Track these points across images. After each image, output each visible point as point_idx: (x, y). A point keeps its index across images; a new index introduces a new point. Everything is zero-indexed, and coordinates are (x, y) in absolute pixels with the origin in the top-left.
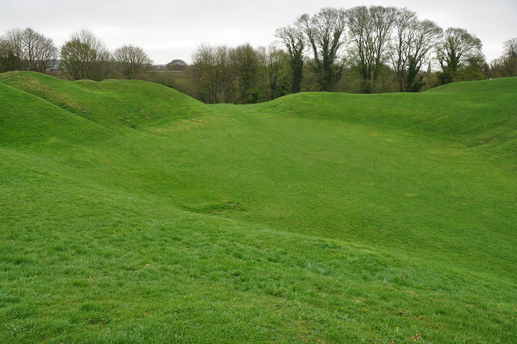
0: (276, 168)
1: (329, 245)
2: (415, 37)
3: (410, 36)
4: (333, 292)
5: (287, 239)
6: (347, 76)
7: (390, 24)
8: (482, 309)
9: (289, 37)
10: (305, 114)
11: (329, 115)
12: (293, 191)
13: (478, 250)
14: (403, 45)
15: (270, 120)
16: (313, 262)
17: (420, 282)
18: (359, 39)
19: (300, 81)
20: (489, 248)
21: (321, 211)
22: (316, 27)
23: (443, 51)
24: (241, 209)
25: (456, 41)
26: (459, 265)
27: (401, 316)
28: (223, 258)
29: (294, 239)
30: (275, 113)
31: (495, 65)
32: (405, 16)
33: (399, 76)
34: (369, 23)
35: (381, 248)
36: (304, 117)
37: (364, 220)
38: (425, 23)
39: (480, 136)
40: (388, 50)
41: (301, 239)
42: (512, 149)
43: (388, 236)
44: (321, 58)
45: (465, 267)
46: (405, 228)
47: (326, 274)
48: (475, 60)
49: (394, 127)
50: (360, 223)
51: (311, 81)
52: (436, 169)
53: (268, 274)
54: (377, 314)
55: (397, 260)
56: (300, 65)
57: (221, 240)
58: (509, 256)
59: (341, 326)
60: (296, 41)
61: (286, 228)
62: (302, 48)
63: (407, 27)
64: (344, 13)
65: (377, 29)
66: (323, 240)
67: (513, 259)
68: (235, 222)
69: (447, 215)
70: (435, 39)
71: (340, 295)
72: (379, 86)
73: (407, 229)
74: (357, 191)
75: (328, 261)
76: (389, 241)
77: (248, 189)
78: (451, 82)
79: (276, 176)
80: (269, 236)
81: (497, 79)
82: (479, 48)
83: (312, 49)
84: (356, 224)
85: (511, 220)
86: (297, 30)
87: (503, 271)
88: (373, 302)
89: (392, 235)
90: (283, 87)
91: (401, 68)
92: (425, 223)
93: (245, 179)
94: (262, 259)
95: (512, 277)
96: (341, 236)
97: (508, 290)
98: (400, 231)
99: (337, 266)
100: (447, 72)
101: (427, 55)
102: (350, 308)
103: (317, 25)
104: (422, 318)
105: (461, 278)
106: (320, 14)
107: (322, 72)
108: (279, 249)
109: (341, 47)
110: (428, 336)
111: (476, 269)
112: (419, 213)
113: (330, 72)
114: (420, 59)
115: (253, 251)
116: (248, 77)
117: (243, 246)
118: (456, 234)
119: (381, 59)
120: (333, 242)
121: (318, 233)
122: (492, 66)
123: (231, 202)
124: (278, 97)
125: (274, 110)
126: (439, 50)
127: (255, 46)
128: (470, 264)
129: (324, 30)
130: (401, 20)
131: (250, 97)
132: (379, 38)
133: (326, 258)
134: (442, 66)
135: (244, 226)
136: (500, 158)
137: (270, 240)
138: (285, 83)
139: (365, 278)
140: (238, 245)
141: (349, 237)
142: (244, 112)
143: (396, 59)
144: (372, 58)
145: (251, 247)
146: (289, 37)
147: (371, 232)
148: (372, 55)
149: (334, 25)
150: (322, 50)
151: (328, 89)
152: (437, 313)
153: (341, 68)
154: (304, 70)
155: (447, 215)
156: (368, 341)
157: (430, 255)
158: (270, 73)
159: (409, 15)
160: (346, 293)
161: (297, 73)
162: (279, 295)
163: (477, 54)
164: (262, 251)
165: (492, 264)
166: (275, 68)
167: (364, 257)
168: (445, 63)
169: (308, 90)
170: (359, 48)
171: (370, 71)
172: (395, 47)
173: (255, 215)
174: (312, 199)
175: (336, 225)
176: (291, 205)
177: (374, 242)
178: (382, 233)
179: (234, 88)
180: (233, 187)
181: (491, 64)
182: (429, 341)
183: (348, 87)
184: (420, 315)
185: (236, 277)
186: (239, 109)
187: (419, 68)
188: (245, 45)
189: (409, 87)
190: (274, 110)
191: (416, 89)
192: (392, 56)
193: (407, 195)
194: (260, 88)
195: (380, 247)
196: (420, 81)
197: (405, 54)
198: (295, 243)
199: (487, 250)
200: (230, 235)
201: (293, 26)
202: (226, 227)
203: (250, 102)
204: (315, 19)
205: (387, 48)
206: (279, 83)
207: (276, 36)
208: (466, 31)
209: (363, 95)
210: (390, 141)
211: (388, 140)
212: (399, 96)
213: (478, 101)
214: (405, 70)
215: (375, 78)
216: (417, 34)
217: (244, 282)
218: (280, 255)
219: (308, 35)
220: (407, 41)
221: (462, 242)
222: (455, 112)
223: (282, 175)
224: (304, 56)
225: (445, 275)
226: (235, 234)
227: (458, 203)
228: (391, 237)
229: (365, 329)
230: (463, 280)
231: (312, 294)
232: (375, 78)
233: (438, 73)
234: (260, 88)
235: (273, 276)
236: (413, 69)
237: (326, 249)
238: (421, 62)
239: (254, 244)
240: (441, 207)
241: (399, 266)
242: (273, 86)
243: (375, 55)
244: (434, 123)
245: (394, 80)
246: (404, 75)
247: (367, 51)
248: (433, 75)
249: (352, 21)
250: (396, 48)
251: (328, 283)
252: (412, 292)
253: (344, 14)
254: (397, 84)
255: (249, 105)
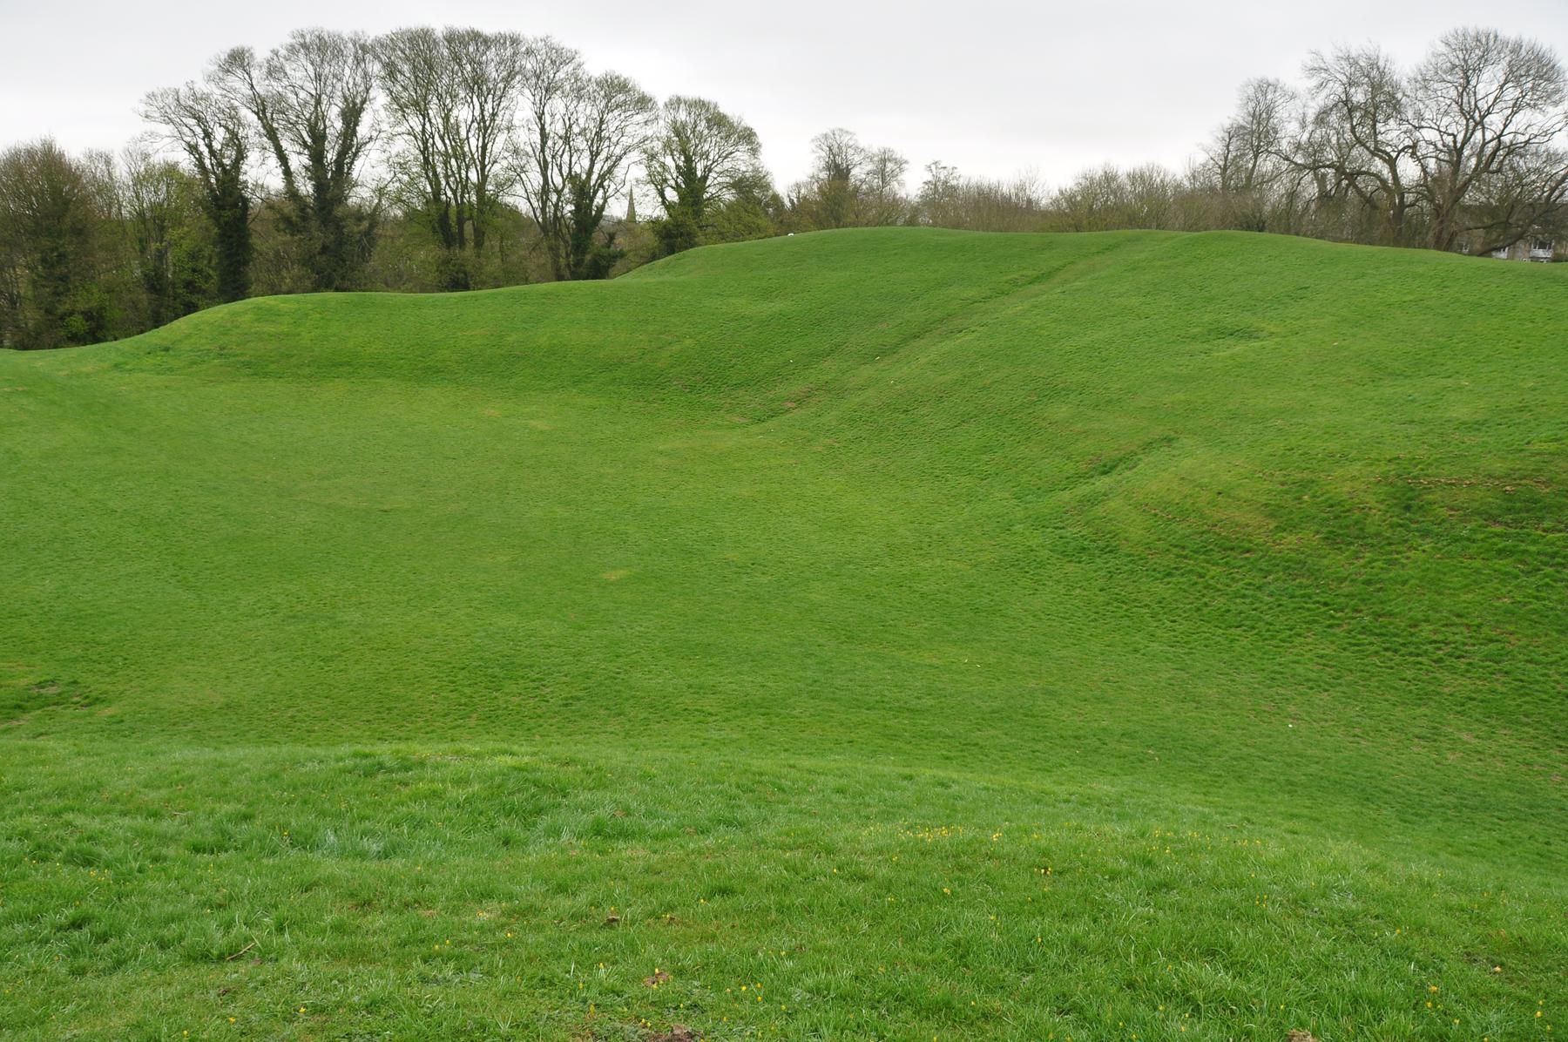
0: (194, 547)
1: (388, 765)
2: (581, 121)
3: (569, 119)
4: (407, 905)
5: (248, 770)
6: (392, 242)
7: (508, 80)
8: (823, 855)
9: (192, 122)
10: (273, 367)
11: (349, 364)
12: (260, 612)
13: (813, 698)
14: (550, 143)
15: (155, 394)
16: (341, 828)
17: (665, 819)
18: (421, 127)
19: (245, 263)
20: (836, 688)
21: (357, 662)
22: (280, 89)
23: (662, 159)
24: (87, 701)
25: (693, 132)
26: (769, 748)
27: (612, 928)
28: (24, 877)
29: (271, 766)
30: (171, 370)
31: (798, 198)
32: (548, 61)
33: (546, 234)
34: (446, 80)
35: (551, 743)
36: (266, 375)
37: (490, 670)
38: (607, 81)
39: (782, 390)
40: (511, 161)
41: (296, 762)
42: (861, 417)
43: (566, 705)
44: (306, 187)
45: (786, 750)
46: (612, 674)
47: (385, 855)
48: (747, 186)
49: (549, 385)
50: (479, 680)
51: (279, 262)
52: (675, 492)
53: (192, 895)
54: (542, 940)
55: (596, 769)
56: (238, 212)
57: (12, 817)
58: (886, 699)
59: (435, 1003)
60: (220, 135)
61: (251, 735)
62: (241, 156)
63: (558, 92)
64: (363, 47)
65: (471, 98)
66: (367, 751)
67: (897, 704)
68: (65, 748)
69: (723, 617)
70: (634, 128)
71: (429, 908)
72: (493, 265)
73: (618, 673)
74: (461, 586)
75: (388, 812)
76: (573, 719)
77: (105, 630)
78: (692, 246)
79: (196, 575)
80: (188, 772)
81: (806, 234)
82: (754, 151)
83: (273, 160)
84: (470, 685)
85: (881, 603)
86: (220, 98)
87: (878, 741)
88: (531, 907)
89: (579, 699)
90: (189, 285)
91: (550, 210)
92: (665, 648)
93: (89, 599)
94: (170, 852)
95: (898, 752)
96: (428, 729)
97: (890, 788)
98: (601, 684)
99: (418, 824)
100: (680, 218)
101: (619, 172)
102: (461, 943)
103: (285, 82)
104: (671, 919)
105: (774, 784)
106: (292, 50)
107: (313, 230)
108: (228, 808)
109: (366, 153)
110: (689, 965)
111: (813, 750)
112: (645, 625)
113: (339, 228)
114: (602, 183)
115: (137, 832)
116: (62, 256)
117: (97, 820)
118: (750, 664)
119: (490, 187)
120: (398, 752)
121: (357, 733)
122: (791, 201)
123: (47, 681)
124: (177, 317)
125: (165, 359)
126: (652, 157)
127: (74, 149)
128: (797, 740)
129: (308, 98)
130: (538, 72)
131: (78, 323)
132: (479, 124)
133: (381, 805)
134: (663, 203)
135: (98, 755)
136: (837, 445)
137: (194, 783)
138: (194, 270)
139: (506, 843)
140: (80, 820)
141: (454, 728)
142: (60, 373)
143: (535, 184)
144: (464, 185)
145: (127, 821)
146: (194, 121)
147: (517, 700)
148: (463, 176)
149: (339, 86)
150: (307, 161)
151: (337, 283)
152: (710, 896)
153: (371, 219)
154: (254, 226)
155: (723, 617)
156: (518, 1026)
157: (691, 736)
158: (141, 241)
159: (559, 58)
160: (447, 898)
161: (231, 237)
162: (232, 955)
163: (751, 168)
164: (167, 826)
165: (850, 728)
166: (154, 222)
167: (498, 780)
168: (672, 195)
169: (274, 290)
170: (423, 153)
171: (460, 222)
172: (529, 149)
173: (139, 712)
174: (324, 629)
175: (409, 699)
176: (258, 658)
177: (529, 730)
178: (549, 697)
179: (11, 295)
180: (48, 632)
181: (789, 196)
182: (694, 978)
183: (400, 275)
184: (666, 912)
185: (76, 934)
186: (39, 364)
187: (601, 209)
188: (38, 145)
189: (578, 264)
190: (165, 359)
191: (599, 270)
192: (523, 175)
193: (605, 576)
194: (108, 292)
195: (549, 739)
196: (609, 247)
197: (560, 170)
198: (276, 777)
199: (833, 693)
200: (46, 796)
201: (202, 87)
202: (32, 769)
203: (76, 339)
204: (275, 63)
205: (506, 154)
206: (174, 272)
207: (147, 117)
208: (716, 107)
209: (449, 294)
210: (540, 424)
211: (533, 423)
212: (551, 294)
213: (766, 295)
214: (563, 216)
215: (479, 244)
216: (588, 112)
217: (105, 941)
218: (230, 827)
219: (257, 114)
220: (562, 132)
221: (769, 684)
222: (710, 329)
223: (216, 568)
224: (250, 181)
225: (730, 786)
226: (65, 789)
227: (745, 579)
228: (578, 705)
229: (509, 995)
230: (779, 789)
231: (339, 928)
232: (479, 244)
233: (655, 222)
234: (109, 291)
235: (209, 900)
236: (586, 212)
237: (380, 777)
238: (605, 193)
239: (138, 809)
240: (702, 598)
241: (601, 785)
242: (155, 283)
243: (473, 176)
244: (659, 365)
245: (535, 247)
246: (560, 230)
247: (446, 163)
248: (642, 228)
249: (391, 71)
250: (531, 153)
251: (391, 881)
252: (641, 853)
253: (364, 51)
254: (545, 259)
255: (75, 351)
